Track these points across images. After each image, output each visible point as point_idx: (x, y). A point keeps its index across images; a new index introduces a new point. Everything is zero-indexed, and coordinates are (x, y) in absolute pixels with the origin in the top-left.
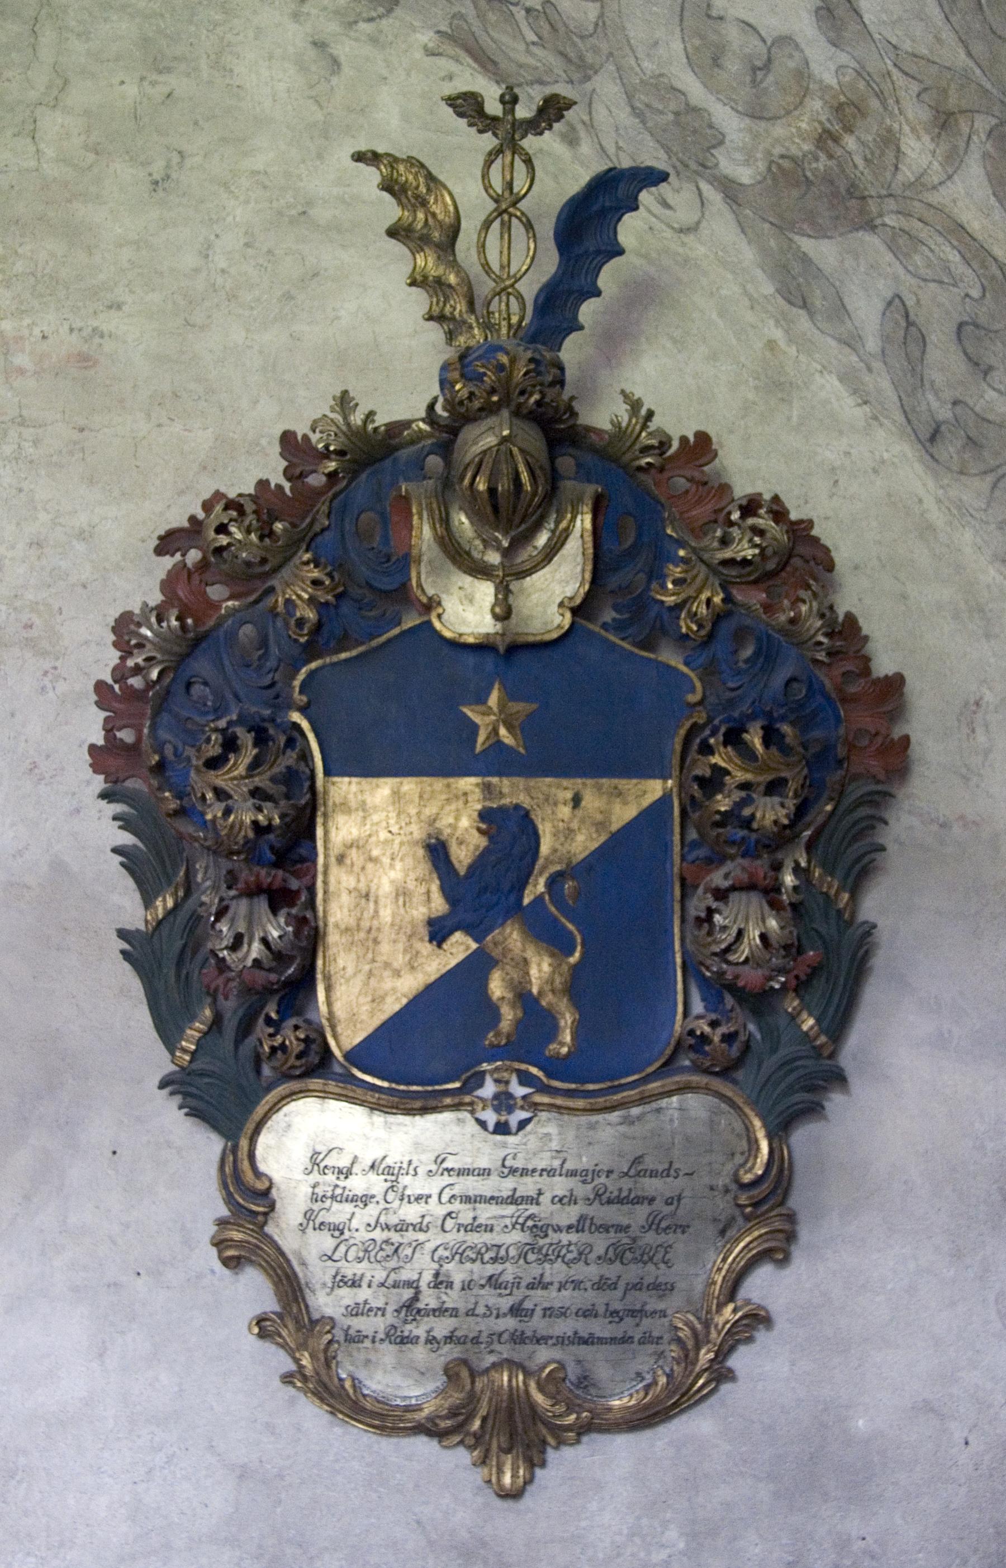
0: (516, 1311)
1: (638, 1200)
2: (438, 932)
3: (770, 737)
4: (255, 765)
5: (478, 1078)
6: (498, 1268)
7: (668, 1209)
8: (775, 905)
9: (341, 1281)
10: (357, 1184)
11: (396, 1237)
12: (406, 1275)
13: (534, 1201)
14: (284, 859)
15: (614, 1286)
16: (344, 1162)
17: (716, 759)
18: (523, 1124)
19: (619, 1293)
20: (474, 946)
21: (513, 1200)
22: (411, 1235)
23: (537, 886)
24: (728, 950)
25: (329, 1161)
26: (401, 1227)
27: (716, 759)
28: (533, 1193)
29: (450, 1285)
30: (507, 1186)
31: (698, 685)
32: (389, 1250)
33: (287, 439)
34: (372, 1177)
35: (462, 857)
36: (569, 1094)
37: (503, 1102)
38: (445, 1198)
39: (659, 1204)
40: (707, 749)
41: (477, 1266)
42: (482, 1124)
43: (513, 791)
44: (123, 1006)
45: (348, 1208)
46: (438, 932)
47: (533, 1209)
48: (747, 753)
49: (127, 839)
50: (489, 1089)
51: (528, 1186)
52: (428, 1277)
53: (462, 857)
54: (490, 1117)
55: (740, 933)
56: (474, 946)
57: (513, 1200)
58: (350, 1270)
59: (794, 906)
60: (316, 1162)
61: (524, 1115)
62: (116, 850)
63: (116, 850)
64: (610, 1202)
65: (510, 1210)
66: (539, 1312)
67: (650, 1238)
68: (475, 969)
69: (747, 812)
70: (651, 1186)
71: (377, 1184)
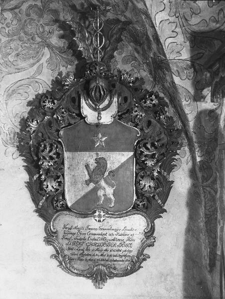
0: (102, 255)
1: (125, 235)
2: (87, 183)
3: (153, 145)
4: (50, 151)
5: (95, 212)
6: (98, 247)
7: (131, 237)
8: (153, 179)
9: (69, 249)
10: (73, 231)
11: (79, 241)
12: (81, 248)
13: (106, 235)
14: (57, 173)
15: (121, 251)
16: (70, 227)
17: (141, 149)
18: (103, 220)
19: (121, 252)
20: (94, 185)
21: (101, 235)
22: (82, 241)
23: (106, 174)
24: (143, 189)
25: (67, 227)
26: (80, 239)
27: (141, 149)
28: (105, 233)
29: (89, 250)
30: (100, 232)
31: (140, 132)
32: (78, 243)
33: (34, 211)
34: (75, 230)
35: (92, 167)
36: (112, 214)
37: (100, 216)
38: (89, 234)
39: (129, 236)
40: (140, 148)
41: (94, 247)
42: (96, 220)
43: (102, 154)
44: (26, 195)
45: (71, 235)
46: (87, 183)
47: (105, 236)
48: (147, 149)
49: (26, 164)
50: (97, 214)
51: (104, 232)
52: (85, 249)
53: (92, 167)
54: (97, 219)
55: (145, 185)
56: (94, 185)
57: (101, 235)
58: (71, 247)
59: (157, 179)
60: (65, 227)
61: (104, 219)
62: (23, 166)
63: (23, 166)
64: (120, 235)
65: (101, 237)
66: (106, 256)
67: (128, 242)
68: (95, 190)
69: (146, 162)
70: (128, 232)
71: (76, 231)
